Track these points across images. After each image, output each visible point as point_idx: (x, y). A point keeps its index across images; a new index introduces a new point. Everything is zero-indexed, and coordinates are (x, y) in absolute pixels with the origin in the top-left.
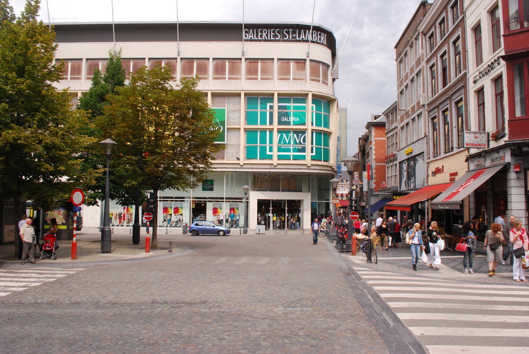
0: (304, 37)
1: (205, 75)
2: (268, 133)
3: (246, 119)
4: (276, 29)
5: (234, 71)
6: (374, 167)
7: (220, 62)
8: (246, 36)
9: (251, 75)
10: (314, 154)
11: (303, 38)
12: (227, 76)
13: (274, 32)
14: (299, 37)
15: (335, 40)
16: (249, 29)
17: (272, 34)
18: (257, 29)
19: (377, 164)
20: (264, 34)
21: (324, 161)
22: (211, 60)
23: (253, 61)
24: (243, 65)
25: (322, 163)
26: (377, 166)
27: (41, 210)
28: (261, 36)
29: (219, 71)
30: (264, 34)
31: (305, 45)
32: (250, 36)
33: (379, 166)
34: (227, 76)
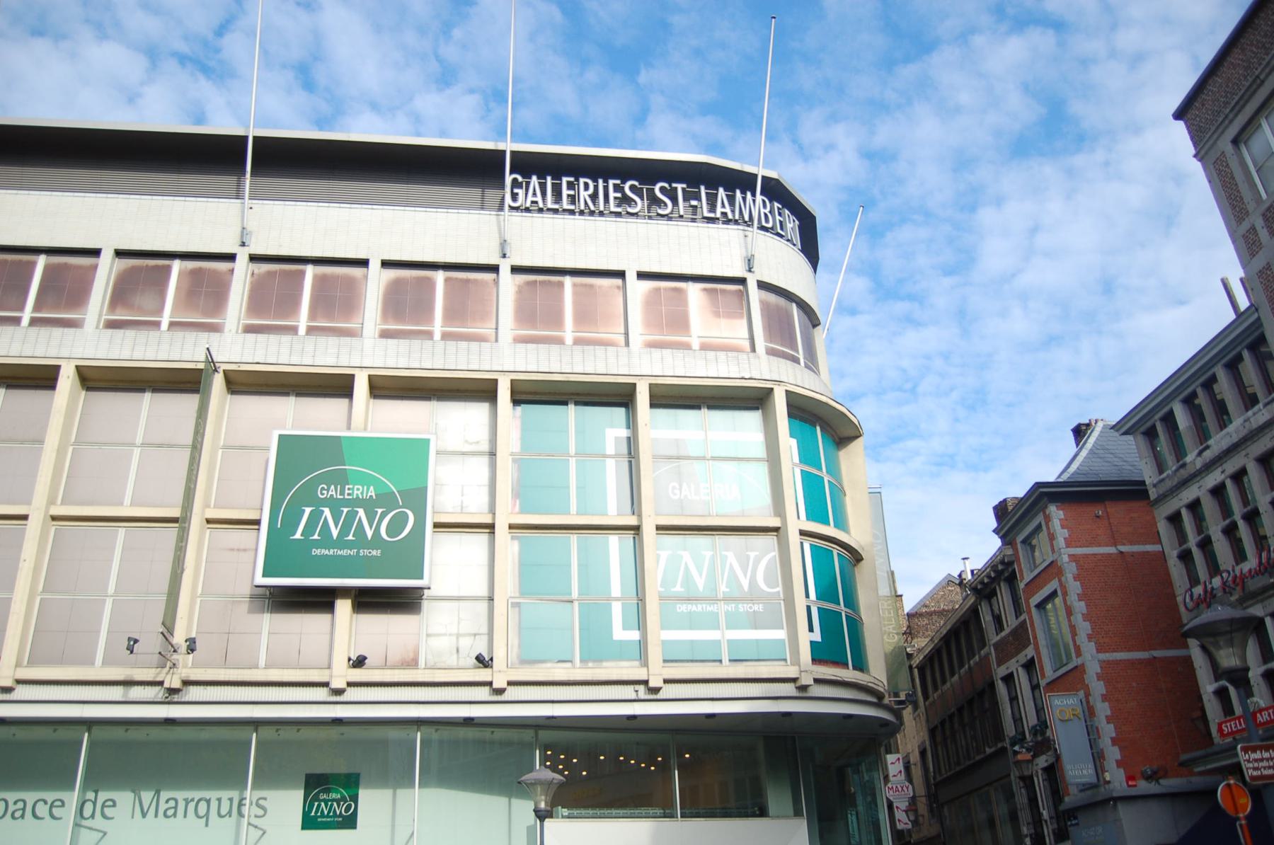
0: (728, 210)
1: (347, 321)
2: (200, 591)
3: (517, 494)
4: (624, 182)
5: (337, 303)
6: (1093, 669)
7: (144, 265)
8: (514, 197)
9: (535, 328)
10: (817, 636)
11: (724, 214)
12: (438, 327)
13: (618, 188)
14: (712, 208)
15: (814, 218)
16: (527, 175)
17: (612, 195)
18: (557, 176)
19: (1103, 656)
20: (584, 195)
21: (855, 668)
22: (375, 265)
23: (284, 265)
24: (242, 275)
25: (849, 674)
26: (1105, 665)
27: (1232, 690)
28: (573, 199)
29: (406, 306)
30: (584, 195)
31: (733, 232)
32: (530, 198)
33: (1117, 662)
34: (438, 327)
